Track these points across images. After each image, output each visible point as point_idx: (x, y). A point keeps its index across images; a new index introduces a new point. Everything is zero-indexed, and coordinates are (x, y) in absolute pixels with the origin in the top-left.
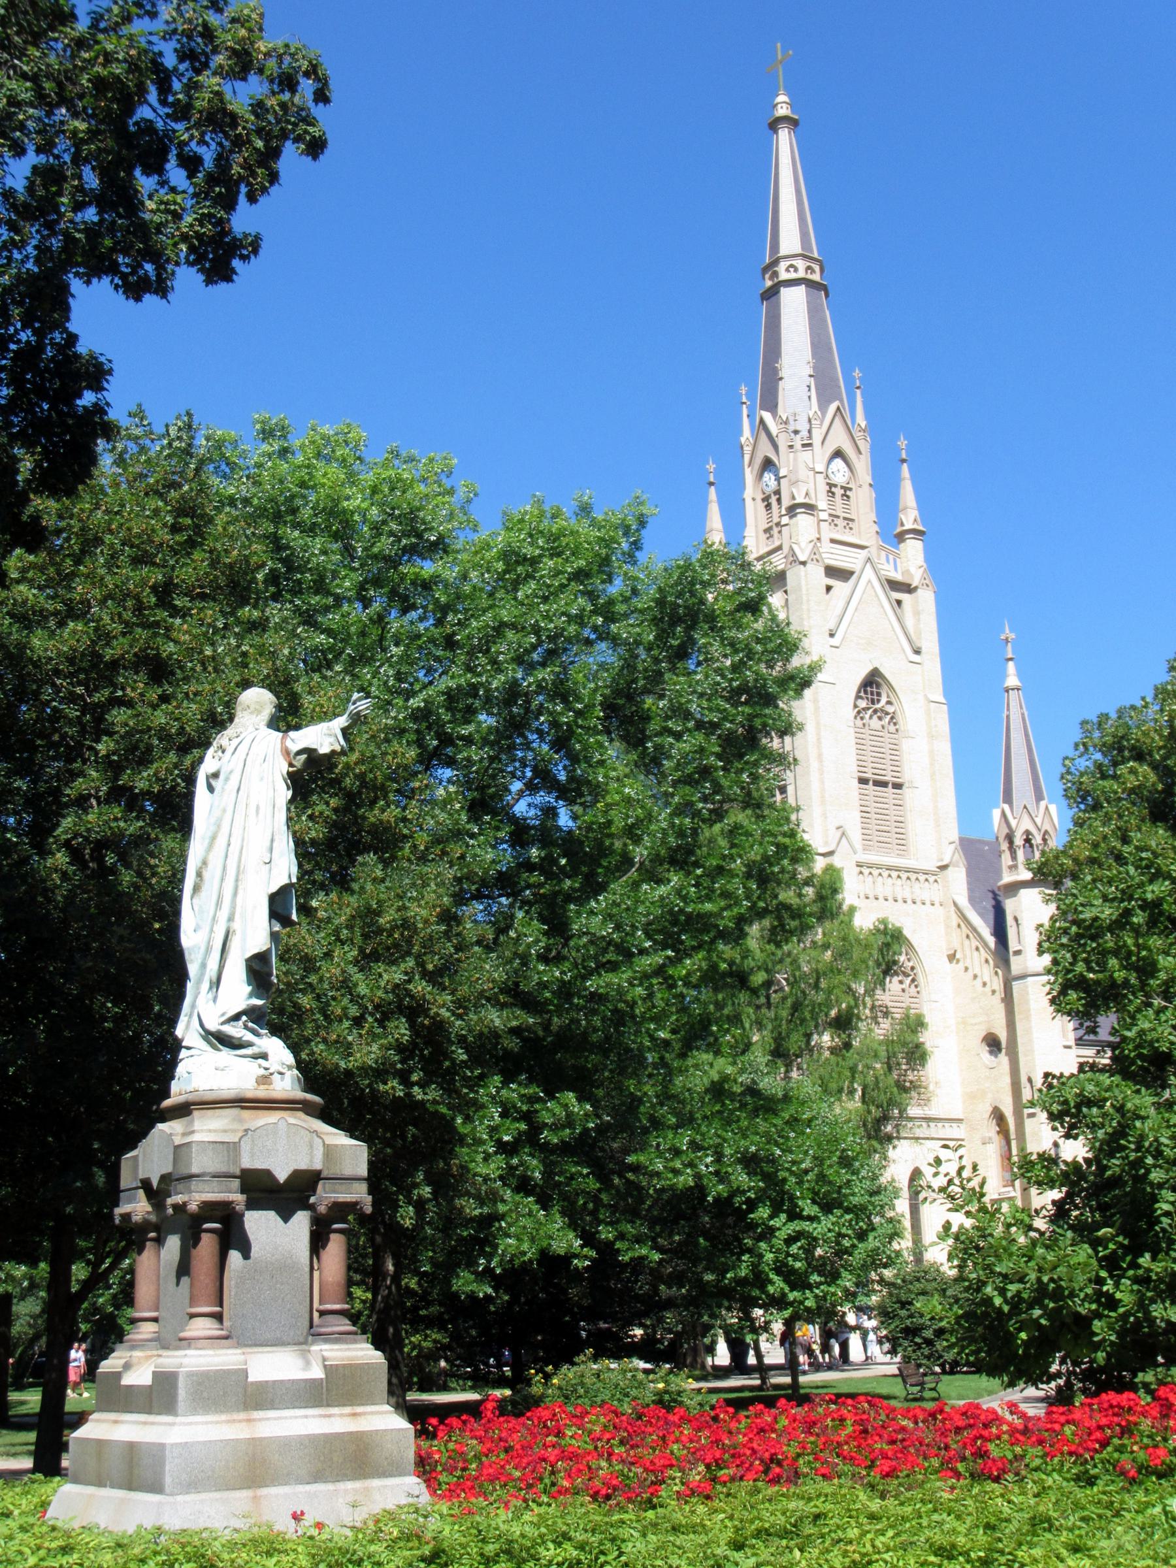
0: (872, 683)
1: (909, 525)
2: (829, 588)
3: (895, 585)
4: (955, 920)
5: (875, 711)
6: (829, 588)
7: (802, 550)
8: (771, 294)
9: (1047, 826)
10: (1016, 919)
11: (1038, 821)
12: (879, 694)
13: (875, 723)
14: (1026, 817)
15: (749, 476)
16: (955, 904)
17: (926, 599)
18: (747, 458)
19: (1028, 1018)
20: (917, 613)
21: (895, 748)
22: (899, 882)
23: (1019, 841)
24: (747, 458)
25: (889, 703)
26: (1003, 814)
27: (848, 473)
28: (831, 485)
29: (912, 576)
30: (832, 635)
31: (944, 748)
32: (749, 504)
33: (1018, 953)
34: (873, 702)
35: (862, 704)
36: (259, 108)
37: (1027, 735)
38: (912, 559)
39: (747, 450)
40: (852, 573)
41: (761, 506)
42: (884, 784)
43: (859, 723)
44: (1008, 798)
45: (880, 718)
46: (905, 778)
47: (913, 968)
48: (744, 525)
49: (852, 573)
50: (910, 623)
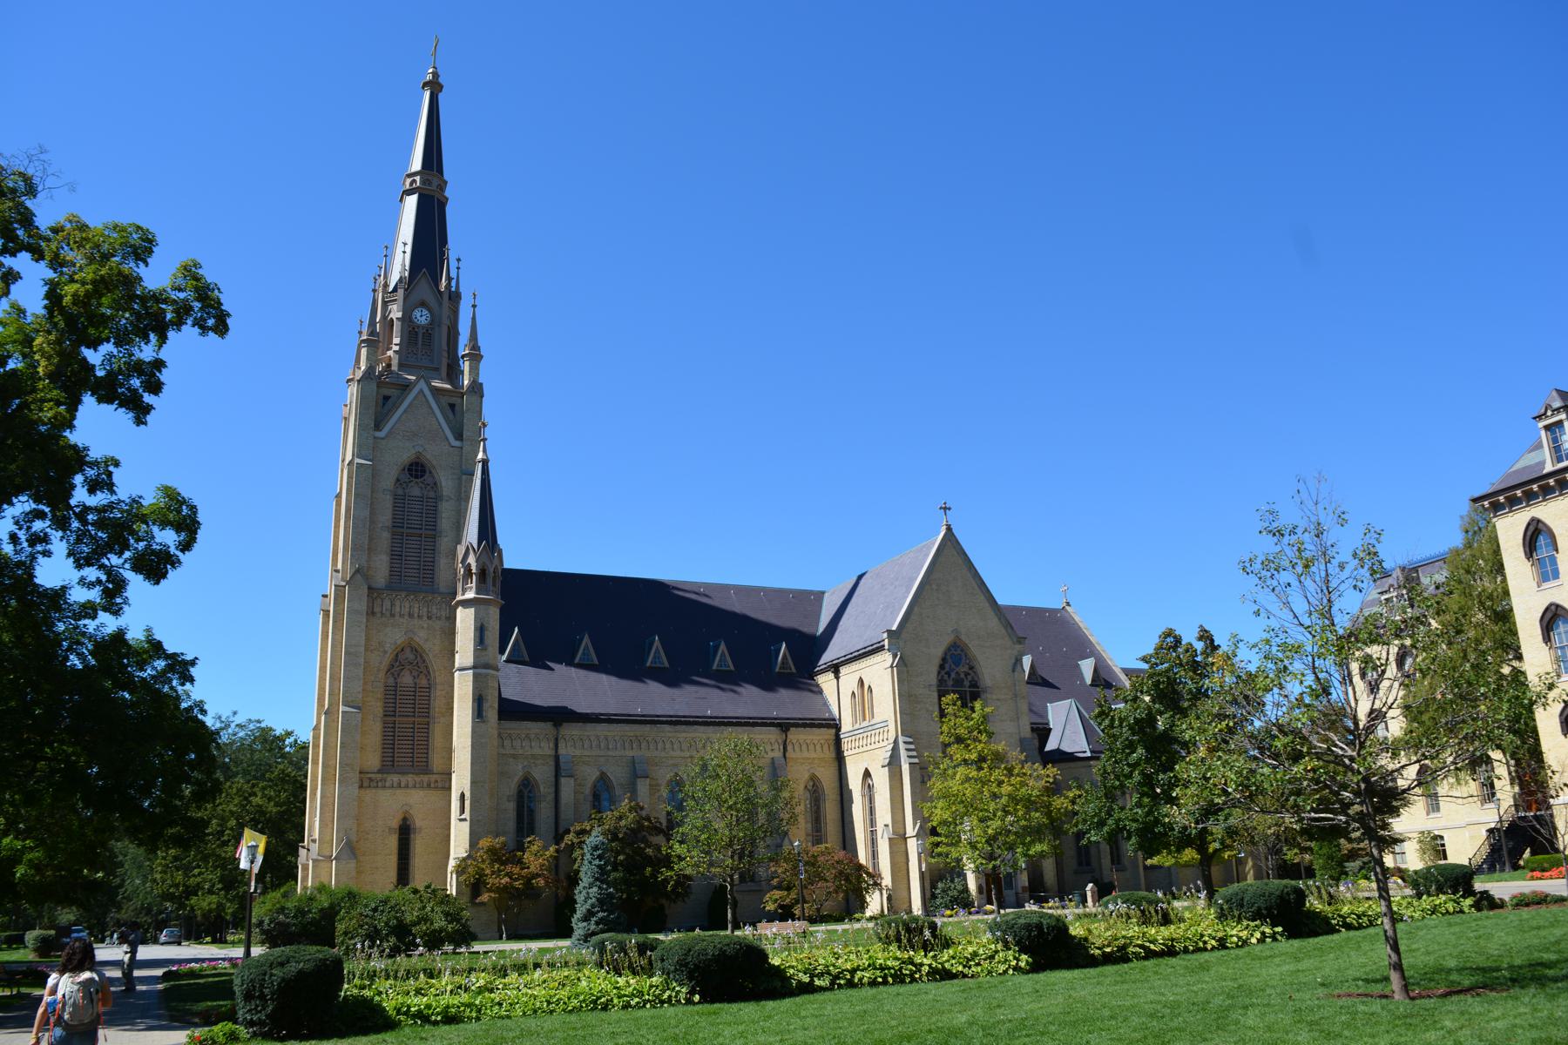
13: (416, 491)
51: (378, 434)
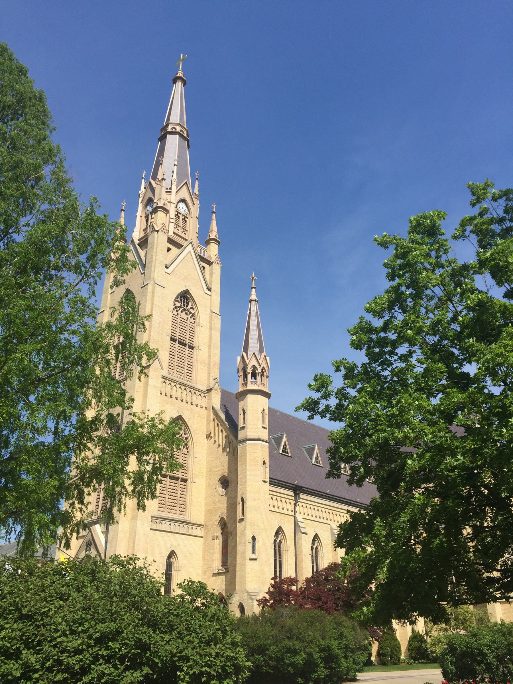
0: (184, 297)
1: (213, 236)
2: (169, 250)
3: (202, 259)
4: (212, 416)
5: (185, 310)
6: (169, 250)
7: (157, 226)
8: (163, 139)
9: (264, 365)
10: (244, 410)
11: (260, 361)
12: (188, 303)
13: (183, 315)
14: (254, 358)
15: (140, 206)
16: (213, 408)
17: (217, 268)
18: (141, 199)
19: (245, 464)
20: (211, 274)
21: (192, 330)
22: (185, 392)
23: (249, 370)
24: (141, 199)
25: (192, 308)
26: (243, 356)
27: (187, 211)
28: (178, 213)
29: (211, 258)
30: (167, 267)
31: (217, 335)
32: (138, 218)
33: (243, 428)
34: (184, 305)
35: (178, 304)
36: (203, 604)
37: (258, 325)
38: (213, 251)
39: (141, 196)
40: (183, 246)
41: (144, 220)
42: (185, 345)
43: (175, 312)
44: (246, 350)
45: (186, 314)
46: (195, 344)
47: (186, 438)
48: (134, 226)
49: (183, 246)
50: (207, 277)
51: (166, 270)
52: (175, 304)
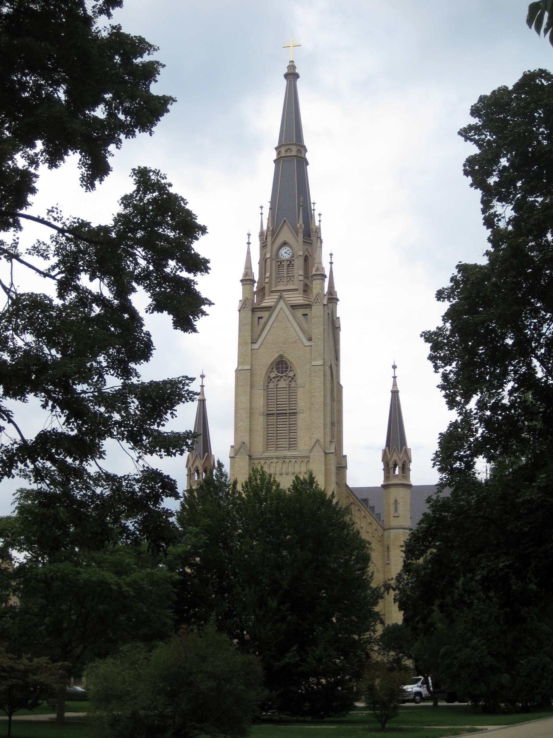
51: (256, 346)
52: (269, 377)
